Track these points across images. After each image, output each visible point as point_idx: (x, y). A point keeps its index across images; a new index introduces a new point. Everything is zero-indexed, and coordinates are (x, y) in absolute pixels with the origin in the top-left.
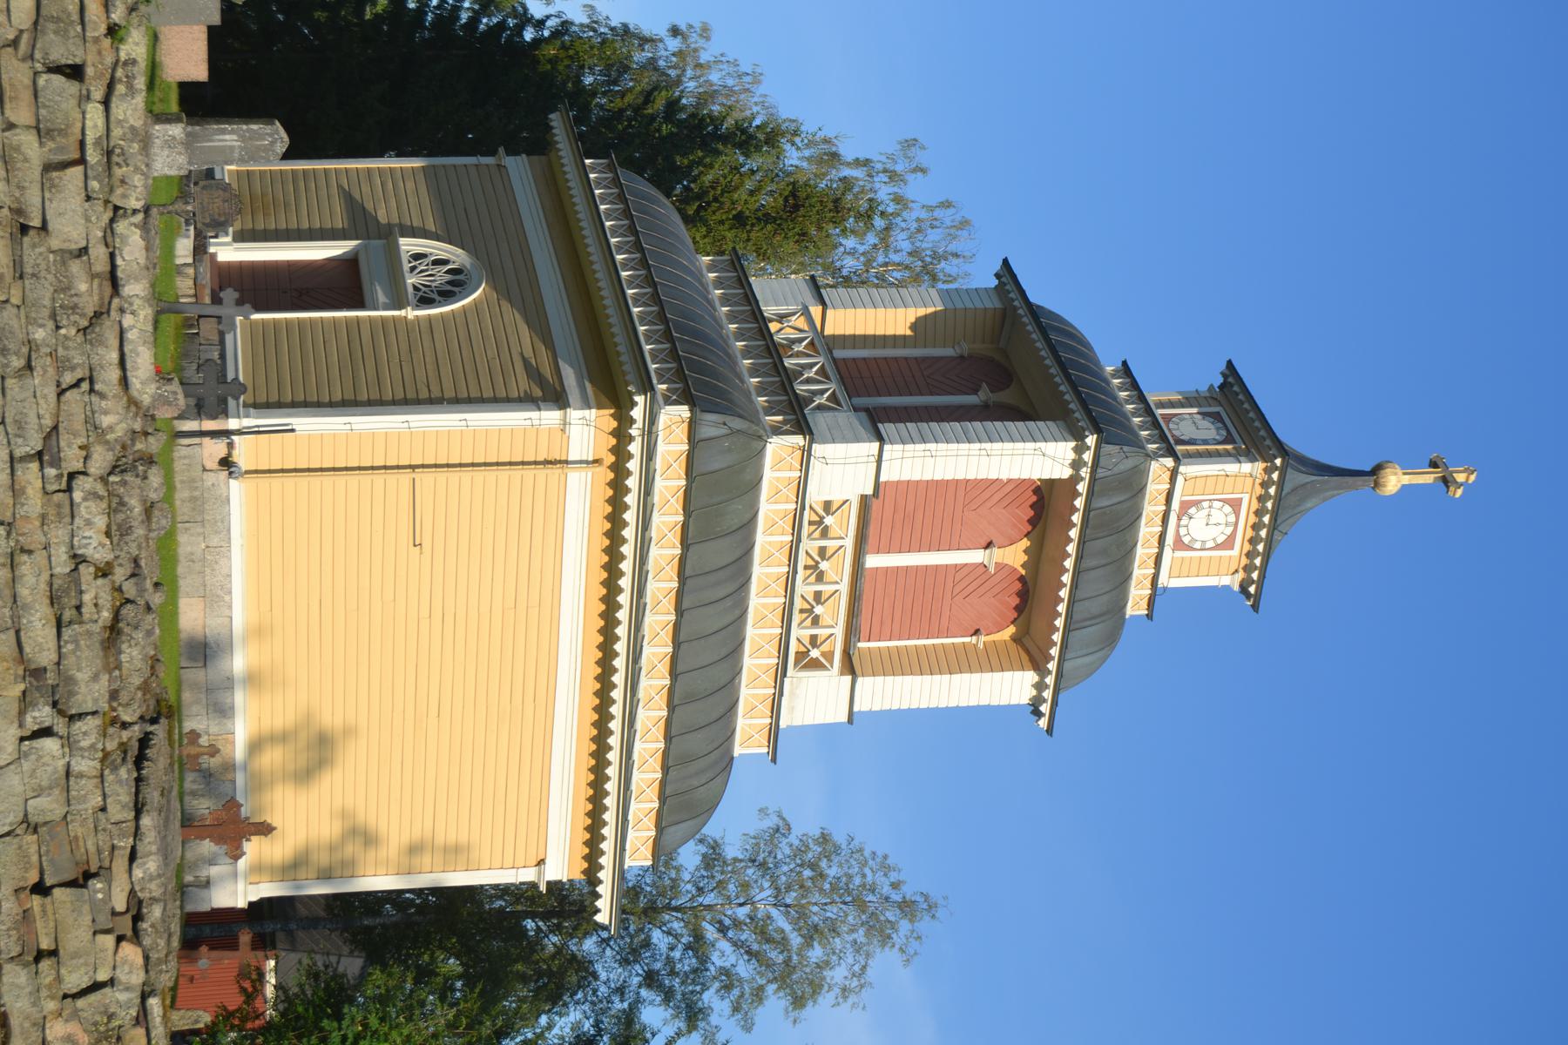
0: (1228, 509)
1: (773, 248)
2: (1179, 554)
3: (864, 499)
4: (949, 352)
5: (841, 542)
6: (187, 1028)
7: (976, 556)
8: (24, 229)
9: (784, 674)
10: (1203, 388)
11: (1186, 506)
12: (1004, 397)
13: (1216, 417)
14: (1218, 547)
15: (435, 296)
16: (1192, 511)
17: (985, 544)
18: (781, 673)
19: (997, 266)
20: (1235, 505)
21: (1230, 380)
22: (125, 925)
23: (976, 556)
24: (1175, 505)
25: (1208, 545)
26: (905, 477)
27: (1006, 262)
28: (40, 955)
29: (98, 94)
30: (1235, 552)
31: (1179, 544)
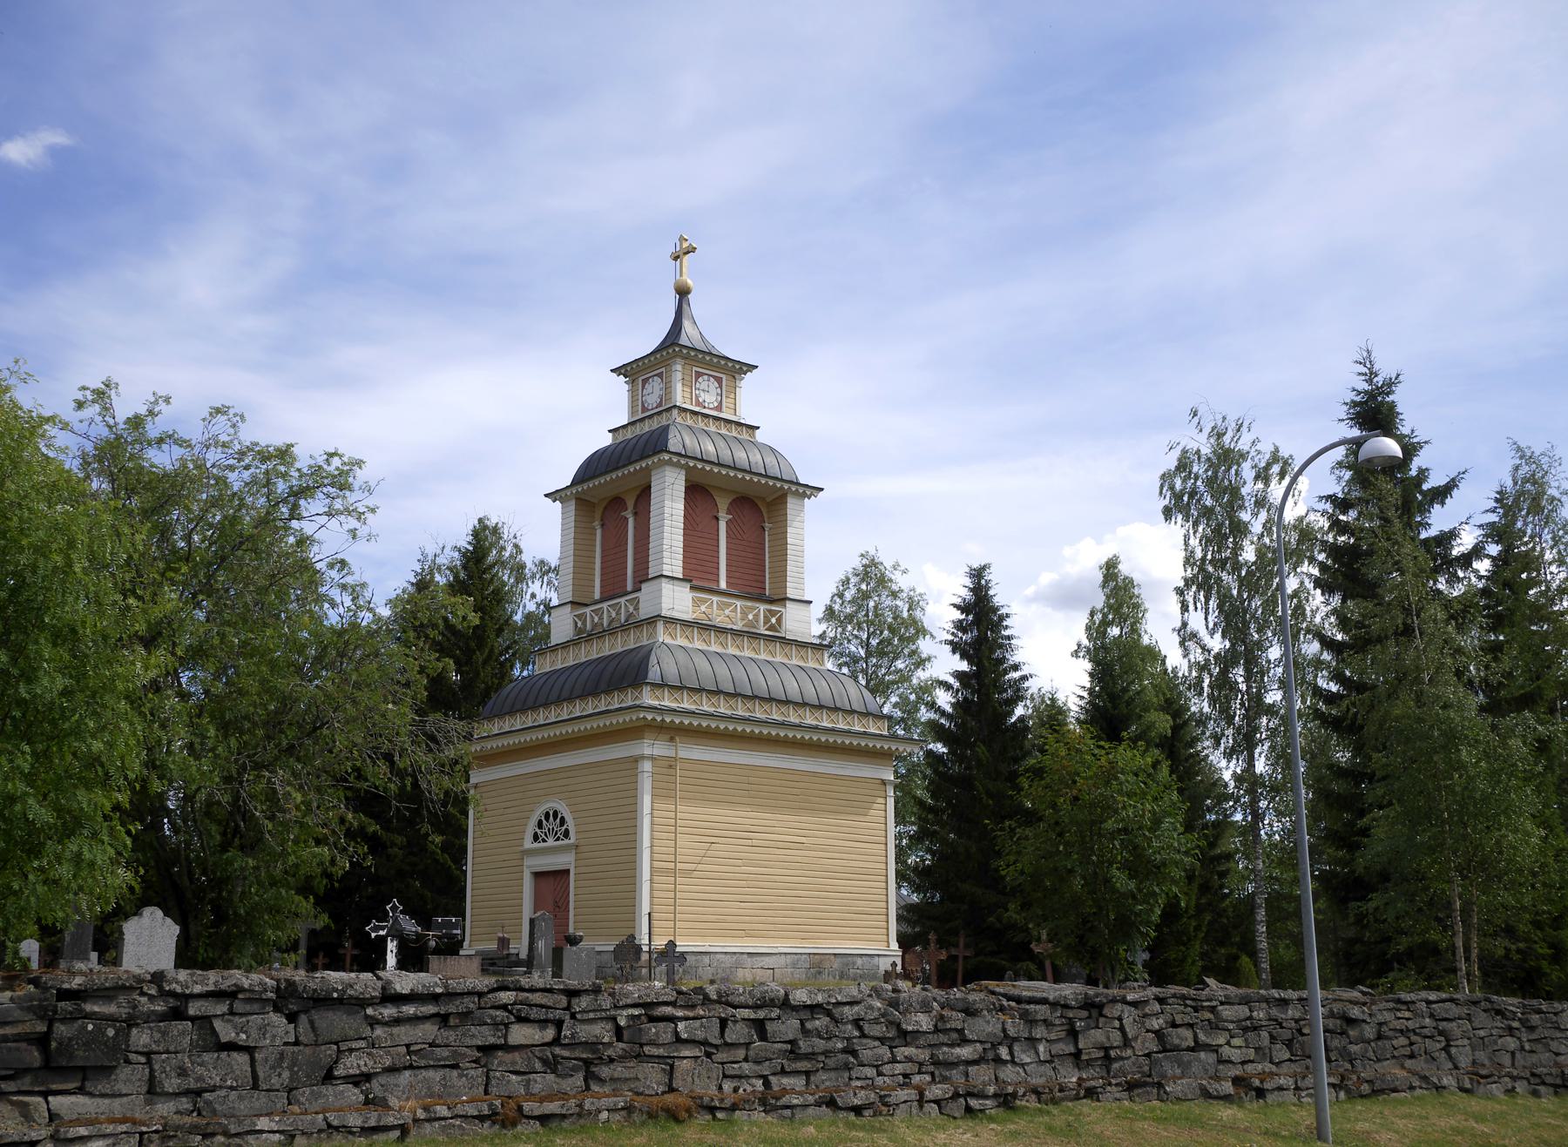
0: (700, 380)
1: (1463, 795)
2: (724, 409)
3: (693, 588)
4: (599, 532)
5: (715, 603)
6: (1062, 985)
7: (723, 526)
8: (792, 1052)
9: (784, 638)
10: (626, 387)
11: (698, 404)
12: (630, 503)
13: (645, 381)
14: (721, 387)
15: (563, 828)
16: (701, 400)
17: (714, 521)
18: (785, 642)
19: (549, 501)
20: (699, 375)
21: (623, 371)
22: (1095, 1013)
23: (723, 526)
24: (697, 409)
25: (719, 392)
26: (681, 563)
27: (546, 495)
28: (1107, 1057)
29: (731, 1010)
30: (724, 376)
31: (719, 408)
